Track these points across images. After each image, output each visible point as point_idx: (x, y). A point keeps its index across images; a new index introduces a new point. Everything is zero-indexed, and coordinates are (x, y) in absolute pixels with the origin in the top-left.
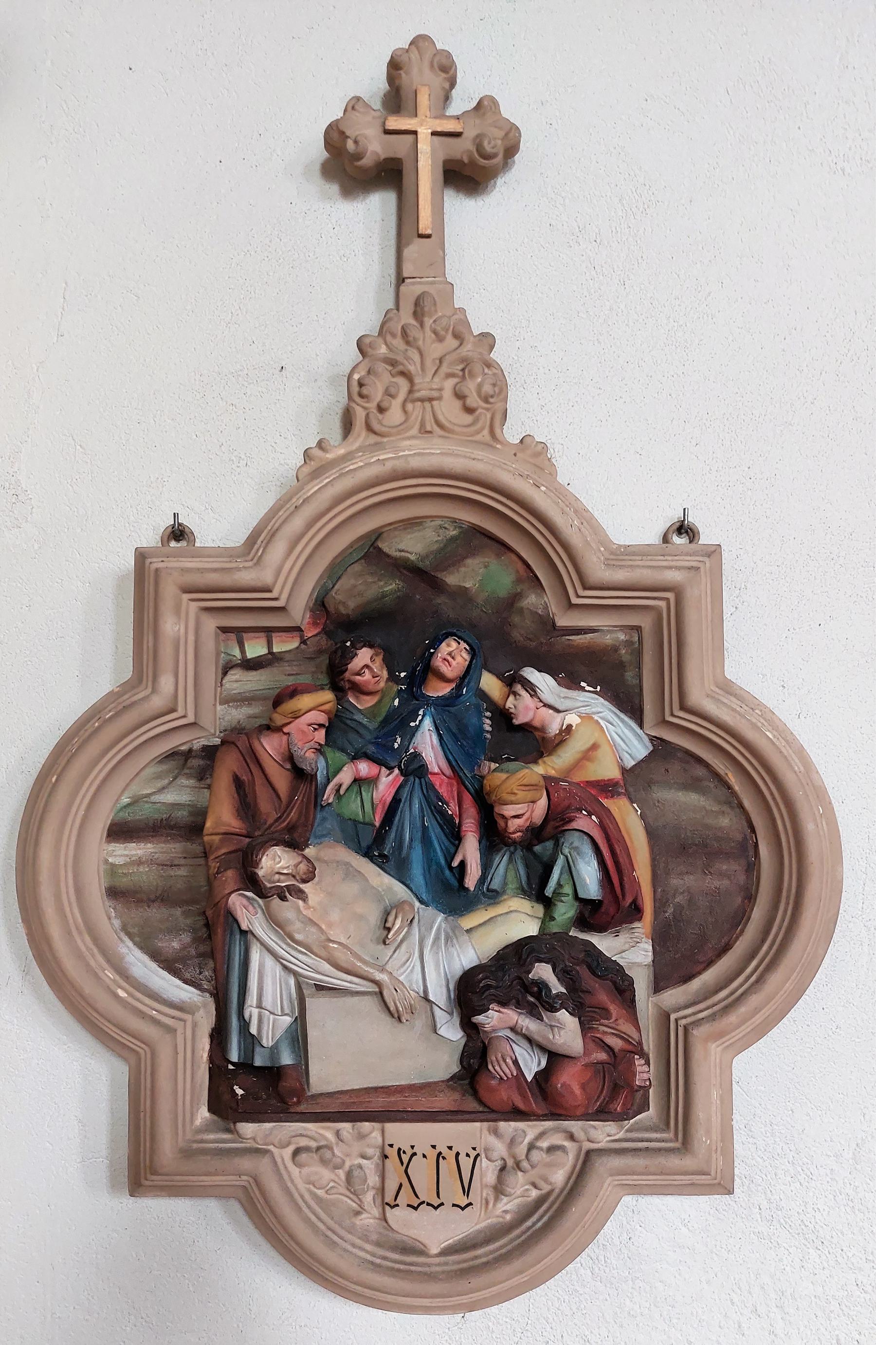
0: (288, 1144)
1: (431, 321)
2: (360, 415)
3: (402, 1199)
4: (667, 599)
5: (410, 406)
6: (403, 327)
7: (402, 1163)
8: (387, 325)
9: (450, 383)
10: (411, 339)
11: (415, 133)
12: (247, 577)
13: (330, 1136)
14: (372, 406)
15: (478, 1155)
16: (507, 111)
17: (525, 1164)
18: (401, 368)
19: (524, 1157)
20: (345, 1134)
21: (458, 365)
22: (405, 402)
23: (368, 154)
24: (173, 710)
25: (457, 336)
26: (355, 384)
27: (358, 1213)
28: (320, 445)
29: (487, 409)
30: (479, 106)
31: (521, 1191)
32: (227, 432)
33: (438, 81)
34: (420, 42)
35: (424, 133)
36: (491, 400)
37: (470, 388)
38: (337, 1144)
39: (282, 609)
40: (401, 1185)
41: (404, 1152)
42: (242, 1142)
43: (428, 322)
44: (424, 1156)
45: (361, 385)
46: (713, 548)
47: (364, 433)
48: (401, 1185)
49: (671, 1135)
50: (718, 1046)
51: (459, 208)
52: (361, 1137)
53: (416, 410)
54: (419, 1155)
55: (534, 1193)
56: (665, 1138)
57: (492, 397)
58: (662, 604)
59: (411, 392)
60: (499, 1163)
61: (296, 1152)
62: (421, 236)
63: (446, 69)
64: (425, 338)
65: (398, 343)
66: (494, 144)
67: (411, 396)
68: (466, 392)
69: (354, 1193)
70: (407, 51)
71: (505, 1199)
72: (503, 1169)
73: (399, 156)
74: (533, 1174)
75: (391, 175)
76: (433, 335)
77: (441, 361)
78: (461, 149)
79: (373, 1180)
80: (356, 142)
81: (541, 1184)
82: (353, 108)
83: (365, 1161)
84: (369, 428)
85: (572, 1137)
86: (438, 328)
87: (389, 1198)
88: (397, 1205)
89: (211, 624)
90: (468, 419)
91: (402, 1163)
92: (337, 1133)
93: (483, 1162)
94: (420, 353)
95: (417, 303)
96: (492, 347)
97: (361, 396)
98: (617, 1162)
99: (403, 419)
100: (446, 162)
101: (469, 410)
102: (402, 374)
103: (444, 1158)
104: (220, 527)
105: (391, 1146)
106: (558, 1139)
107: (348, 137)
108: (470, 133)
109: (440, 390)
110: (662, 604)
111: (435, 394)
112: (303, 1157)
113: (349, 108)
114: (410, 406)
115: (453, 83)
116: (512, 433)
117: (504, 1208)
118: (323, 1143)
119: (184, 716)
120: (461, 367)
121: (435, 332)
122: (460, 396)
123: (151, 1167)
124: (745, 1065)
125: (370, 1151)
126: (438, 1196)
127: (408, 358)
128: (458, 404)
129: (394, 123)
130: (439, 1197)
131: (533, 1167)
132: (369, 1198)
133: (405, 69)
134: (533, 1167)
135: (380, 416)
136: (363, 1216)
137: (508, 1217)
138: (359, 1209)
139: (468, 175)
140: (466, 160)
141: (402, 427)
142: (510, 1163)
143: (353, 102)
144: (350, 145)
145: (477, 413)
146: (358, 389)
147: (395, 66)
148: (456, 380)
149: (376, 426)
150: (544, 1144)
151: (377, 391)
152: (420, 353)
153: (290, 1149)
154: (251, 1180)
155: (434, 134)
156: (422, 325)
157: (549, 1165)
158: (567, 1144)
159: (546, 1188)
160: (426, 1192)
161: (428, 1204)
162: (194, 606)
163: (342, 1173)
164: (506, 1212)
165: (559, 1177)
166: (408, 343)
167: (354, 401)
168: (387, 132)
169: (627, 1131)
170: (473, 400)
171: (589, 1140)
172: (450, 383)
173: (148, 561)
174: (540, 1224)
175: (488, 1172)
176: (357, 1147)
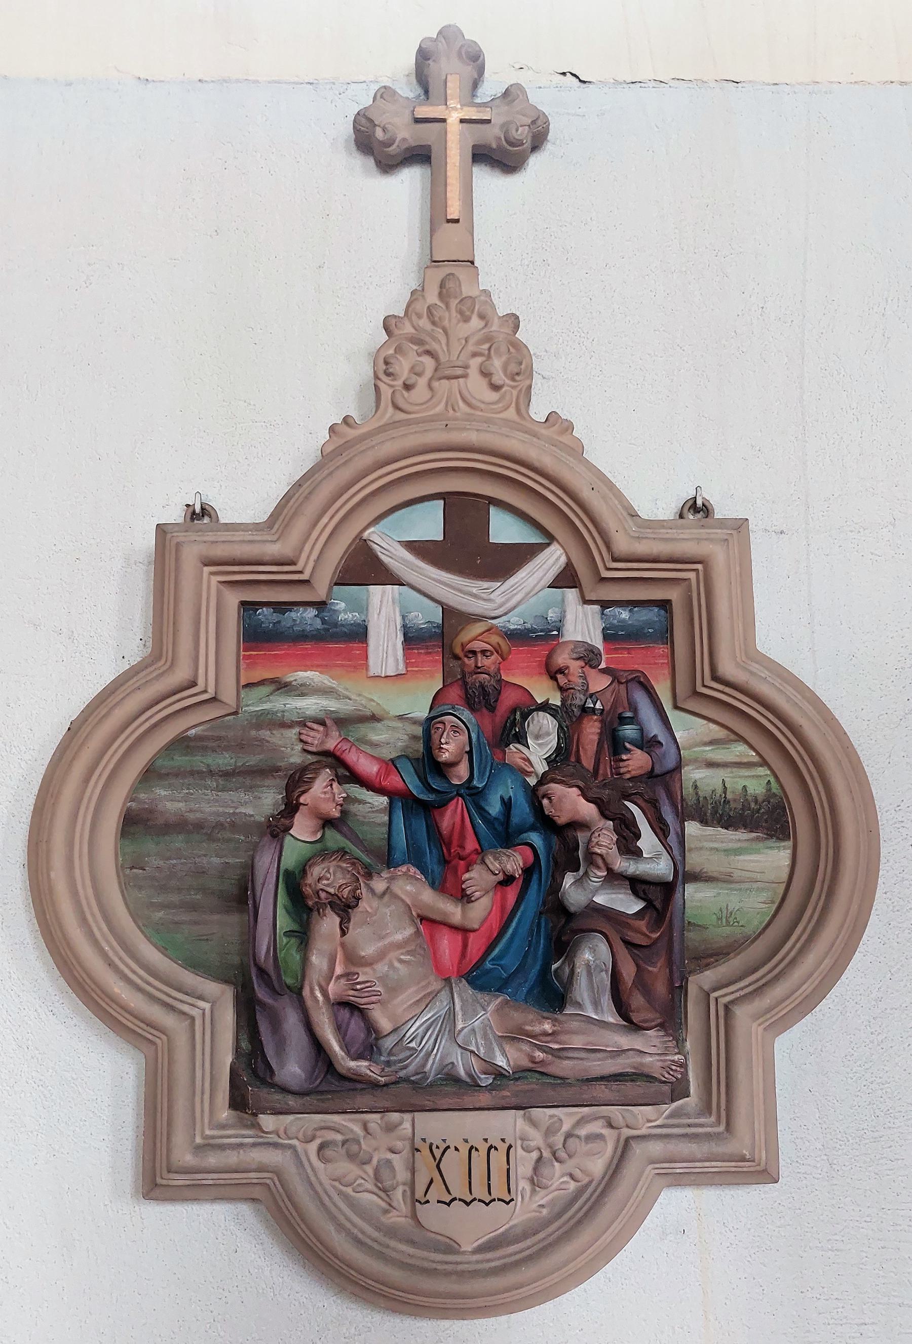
0: (313, 1138)
1: (457, 301)
2: (386, 392)
3: (433, 1195)
4: (696, 570)
5: (436, 384)
6: (428, 307)
7: (435, 1159)
8: (413, 306)
9: (475, 362)
10: (436, 319)
11: (444, 120)
12: (274, 549)
13: (358, 1129)
14: (399, 383)
15: (510, 1147)
16: (534, 98)
17: (562, 1154)
18: (427, 347)
19: (561, 1146)
20: (372, 1126)
21: (483, 344)
22: (431, 380)
23: (398, 140)
24: (194, 684)
25: (482, 317)
26: (381, 361)
27: (386, 1212)
28: (346, 420)
29: (513, 387)
30: (506, 94)
31: (560, 1182)
32: (254, 422)
33: (469, 71)
34: (448, 34)
35: (453, 118)
36: (517, 378)
37: (497, 364)
38: (364, 1137)
39: (307, 582)
40: (431, 1182)
41: (438, 1147)
42: (262, 1137)
43: (454, 303)
44: (456, 1149)
45: (386, 363)
46: (741, 522)
47: (391, 410)
48: (431, 1182)
49: (713, 1119)
50: (759, 1025)
51: (486, 180)
52: (390, 1128)
53: (442, 386)
54: (452, 1148)
55: (572, 1186)
56: (709, 1124)
57: (518, 374)
58: (692, 576)
59: (436, 370)
60: (535, 1155)
61: (321, 1147)
62: (449, 221)
63: (475, 59)
64: (450, 318)
65: (424, 323)
66: (522, 134)
67: (439, 374)
68: (493, 370)
69: (385, 1191)
70: (436, 40)
71: (542, 1192)
72: (540, 1159)
73: (429, 143)
74: (570, 1165)
75: (420, 156)
76: (459, 316)
77: (466, 340)
78: (491, 135)
79: (402, 1174)
80: (384, 130)
81: (578, 1173)
82: (382, 97)
83: (393, 1156)
84: (396, 407)
85: (610, 1126)
86: (464, 308)
87: (419, 1194)
88: (428, 1202)
89: (233, 599)
90: (494, 396)
91: (435, 1159)
92: (365, 1127)
93: (518, 1152)
94: (445, 327)
95: (442, 285)
96: (517, 327)
97: (388, 374)
98: (656, 1148)
99: (429, 397)
100: (474, 147)
101: (496, 388)
102: (428, 353)
103: (496, 1149)
104: (246, 501)
105: (424, 1140)
106: (596, 1127)
107: (375, 125)
108: (497, 120)
109: (466, 367)
110: (692, 576)
111: (459, 372)
112: (328, 1153)
113: (378, 97)
114: (436, 384)
115: (481, 70)
116: (538, 411)
117: (540, 1203)
118: (351, 1136)
119: (205, 691)
120: (486, 346)
121: (461, 312)
122: (485, 374)
123: (168, 1167)
124: (788, 1046)
125: (399, 1145)
126: (471, 1193)
127: (434, 339)
128: (483, 383)
129: (424, 111)
130: (450, 1193)
131: (570, 1156)
132: (398, 1195)
133: (434, 58)
134: (570, 1156)
135: (405, 394)
136: (391, 1214)
137: (545, 1211)
138: (388, 1207)
139: (501, 156)
140: (494, 146)
141: (424, 406)
142: (546, 1154)
143: (383, 90)
144: (379, 134)
145: (504, 389)
146: (384, 368)
147: (424, 56)
148: (483, 359)
149: (401, 403)
150: (583, 1132)
151: (403, 367)
152: (445, 327)
153: (318, 1142)
154: (276, 1178)
155: (462, 121)
156: (447, 306)
157: (590, 1154)
158: (606, 1132)
159: (586, 1180)
160: (458, 1189)
161: (480, 1201)
162: (215, 579)
163: (369, 1169)
164: (542, 1206)
165: (597, 1166)
166: (434, 323)
167: (380, 379)
168: (418, 121)
169: (667, 1118)
170: (499, 377)
171: (628, 1126)
172: (475, 362)
173: (169, 536)
174: (299, 1231)
175: (523, 1163)
176: (385, 1140)
